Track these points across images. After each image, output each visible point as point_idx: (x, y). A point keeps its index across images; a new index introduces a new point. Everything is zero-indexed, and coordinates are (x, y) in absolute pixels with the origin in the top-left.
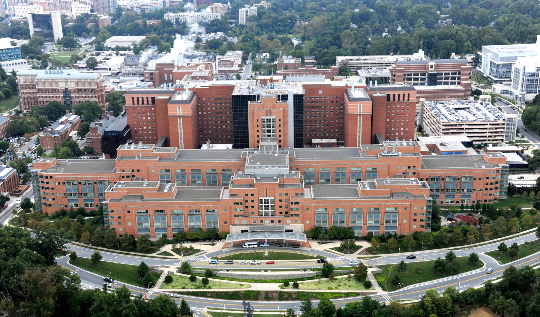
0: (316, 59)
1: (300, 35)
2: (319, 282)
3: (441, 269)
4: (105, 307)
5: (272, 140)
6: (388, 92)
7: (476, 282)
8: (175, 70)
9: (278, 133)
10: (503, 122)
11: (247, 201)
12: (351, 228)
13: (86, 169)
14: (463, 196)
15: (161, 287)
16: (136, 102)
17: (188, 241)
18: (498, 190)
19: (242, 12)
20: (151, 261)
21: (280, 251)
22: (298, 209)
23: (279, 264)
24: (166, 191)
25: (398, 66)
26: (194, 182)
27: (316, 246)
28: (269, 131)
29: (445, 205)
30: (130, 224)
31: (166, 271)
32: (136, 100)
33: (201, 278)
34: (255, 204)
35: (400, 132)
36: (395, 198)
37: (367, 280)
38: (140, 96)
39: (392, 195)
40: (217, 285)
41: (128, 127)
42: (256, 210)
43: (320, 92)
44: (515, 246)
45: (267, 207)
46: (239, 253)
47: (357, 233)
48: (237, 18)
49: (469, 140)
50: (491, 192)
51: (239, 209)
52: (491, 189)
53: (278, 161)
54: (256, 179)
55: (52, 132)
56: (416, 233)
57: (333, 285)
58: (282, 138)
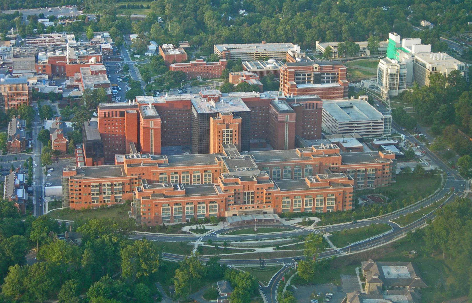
10: (382, 121)
18: (391, 177)
49: (360, 137)
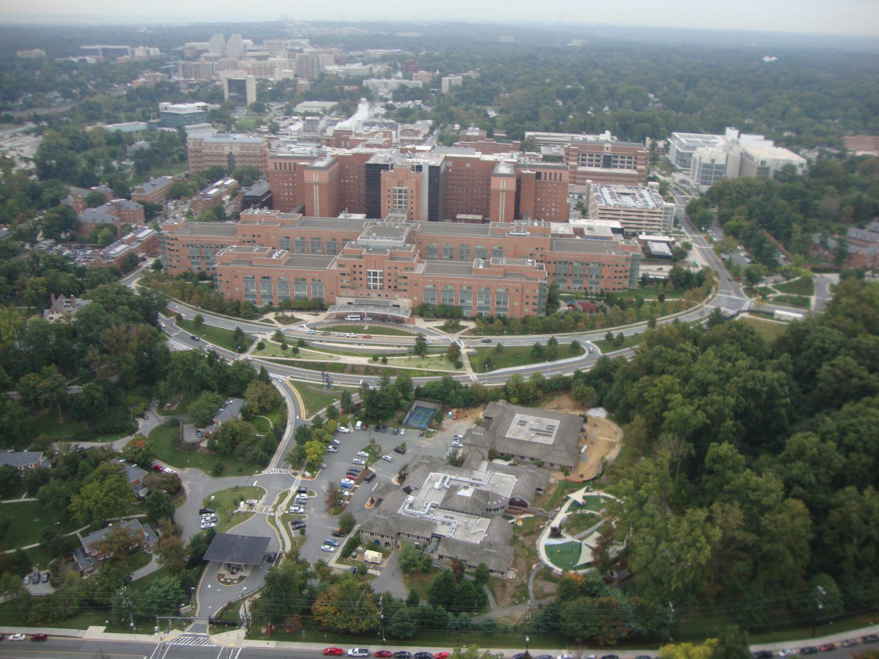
0: (507, 133)
1: (498, 108)
2: (410, 359)
3: (538, 354)
4: (179, 365)
5: (403, 212)
6: (539, 170)
7: (569, 370)
8: (352, 137)
9: (410, 205)
11: (355, 272)
12: (460, 307)
13: (209, 233)
14: (591, 282)
15: (253, 353)
16: (278, 167)
17: (293, 309)
18: (628, 279)
19: (445, 81)
20: (248, 327)
21: (382, 326)
22: (406, 284)
23: (376, 337)
24: (274, 257)
25: (572, 145)
26: (313, 251)
27: (421, 323)
28: (400, 202)
29: (573, 291)
30: (237, 289)
31: (260, 337)
32: (278, 165)
33: (292, 347)
34: (363, 276)
35: (550, 212)
36: (508, 279)
37: (459, 360)
38: (287, 162)
39: (505, 275)
40: (307, 355)
41: (269, 192)
42: (364, 282)
43: (468, 165)
44: (621, 337)
45: (375, 280)
46: (339, 325)
47: (465, 313)
48: (440, 87)
50: (620, 280)
51: (346, 280)
52: (620, 278)
53: (396, 234)
54: (368, 250)
55: (205, 196)
56: (527, 317)
57: (424, 363)
58: (414, 211)
